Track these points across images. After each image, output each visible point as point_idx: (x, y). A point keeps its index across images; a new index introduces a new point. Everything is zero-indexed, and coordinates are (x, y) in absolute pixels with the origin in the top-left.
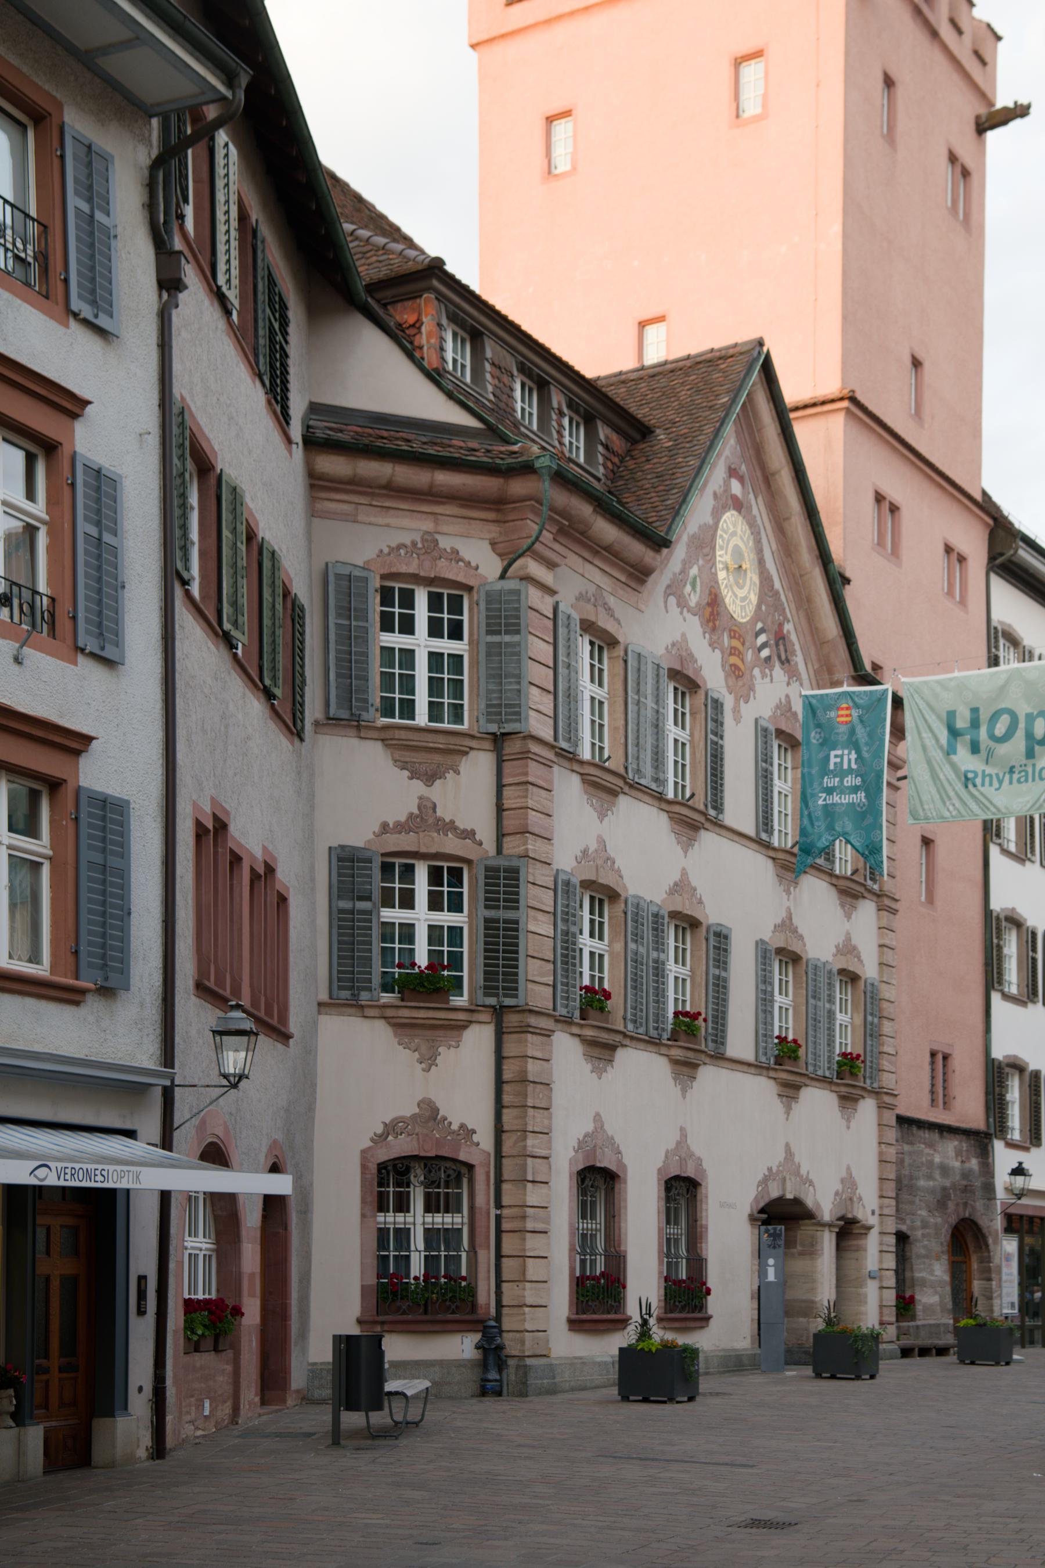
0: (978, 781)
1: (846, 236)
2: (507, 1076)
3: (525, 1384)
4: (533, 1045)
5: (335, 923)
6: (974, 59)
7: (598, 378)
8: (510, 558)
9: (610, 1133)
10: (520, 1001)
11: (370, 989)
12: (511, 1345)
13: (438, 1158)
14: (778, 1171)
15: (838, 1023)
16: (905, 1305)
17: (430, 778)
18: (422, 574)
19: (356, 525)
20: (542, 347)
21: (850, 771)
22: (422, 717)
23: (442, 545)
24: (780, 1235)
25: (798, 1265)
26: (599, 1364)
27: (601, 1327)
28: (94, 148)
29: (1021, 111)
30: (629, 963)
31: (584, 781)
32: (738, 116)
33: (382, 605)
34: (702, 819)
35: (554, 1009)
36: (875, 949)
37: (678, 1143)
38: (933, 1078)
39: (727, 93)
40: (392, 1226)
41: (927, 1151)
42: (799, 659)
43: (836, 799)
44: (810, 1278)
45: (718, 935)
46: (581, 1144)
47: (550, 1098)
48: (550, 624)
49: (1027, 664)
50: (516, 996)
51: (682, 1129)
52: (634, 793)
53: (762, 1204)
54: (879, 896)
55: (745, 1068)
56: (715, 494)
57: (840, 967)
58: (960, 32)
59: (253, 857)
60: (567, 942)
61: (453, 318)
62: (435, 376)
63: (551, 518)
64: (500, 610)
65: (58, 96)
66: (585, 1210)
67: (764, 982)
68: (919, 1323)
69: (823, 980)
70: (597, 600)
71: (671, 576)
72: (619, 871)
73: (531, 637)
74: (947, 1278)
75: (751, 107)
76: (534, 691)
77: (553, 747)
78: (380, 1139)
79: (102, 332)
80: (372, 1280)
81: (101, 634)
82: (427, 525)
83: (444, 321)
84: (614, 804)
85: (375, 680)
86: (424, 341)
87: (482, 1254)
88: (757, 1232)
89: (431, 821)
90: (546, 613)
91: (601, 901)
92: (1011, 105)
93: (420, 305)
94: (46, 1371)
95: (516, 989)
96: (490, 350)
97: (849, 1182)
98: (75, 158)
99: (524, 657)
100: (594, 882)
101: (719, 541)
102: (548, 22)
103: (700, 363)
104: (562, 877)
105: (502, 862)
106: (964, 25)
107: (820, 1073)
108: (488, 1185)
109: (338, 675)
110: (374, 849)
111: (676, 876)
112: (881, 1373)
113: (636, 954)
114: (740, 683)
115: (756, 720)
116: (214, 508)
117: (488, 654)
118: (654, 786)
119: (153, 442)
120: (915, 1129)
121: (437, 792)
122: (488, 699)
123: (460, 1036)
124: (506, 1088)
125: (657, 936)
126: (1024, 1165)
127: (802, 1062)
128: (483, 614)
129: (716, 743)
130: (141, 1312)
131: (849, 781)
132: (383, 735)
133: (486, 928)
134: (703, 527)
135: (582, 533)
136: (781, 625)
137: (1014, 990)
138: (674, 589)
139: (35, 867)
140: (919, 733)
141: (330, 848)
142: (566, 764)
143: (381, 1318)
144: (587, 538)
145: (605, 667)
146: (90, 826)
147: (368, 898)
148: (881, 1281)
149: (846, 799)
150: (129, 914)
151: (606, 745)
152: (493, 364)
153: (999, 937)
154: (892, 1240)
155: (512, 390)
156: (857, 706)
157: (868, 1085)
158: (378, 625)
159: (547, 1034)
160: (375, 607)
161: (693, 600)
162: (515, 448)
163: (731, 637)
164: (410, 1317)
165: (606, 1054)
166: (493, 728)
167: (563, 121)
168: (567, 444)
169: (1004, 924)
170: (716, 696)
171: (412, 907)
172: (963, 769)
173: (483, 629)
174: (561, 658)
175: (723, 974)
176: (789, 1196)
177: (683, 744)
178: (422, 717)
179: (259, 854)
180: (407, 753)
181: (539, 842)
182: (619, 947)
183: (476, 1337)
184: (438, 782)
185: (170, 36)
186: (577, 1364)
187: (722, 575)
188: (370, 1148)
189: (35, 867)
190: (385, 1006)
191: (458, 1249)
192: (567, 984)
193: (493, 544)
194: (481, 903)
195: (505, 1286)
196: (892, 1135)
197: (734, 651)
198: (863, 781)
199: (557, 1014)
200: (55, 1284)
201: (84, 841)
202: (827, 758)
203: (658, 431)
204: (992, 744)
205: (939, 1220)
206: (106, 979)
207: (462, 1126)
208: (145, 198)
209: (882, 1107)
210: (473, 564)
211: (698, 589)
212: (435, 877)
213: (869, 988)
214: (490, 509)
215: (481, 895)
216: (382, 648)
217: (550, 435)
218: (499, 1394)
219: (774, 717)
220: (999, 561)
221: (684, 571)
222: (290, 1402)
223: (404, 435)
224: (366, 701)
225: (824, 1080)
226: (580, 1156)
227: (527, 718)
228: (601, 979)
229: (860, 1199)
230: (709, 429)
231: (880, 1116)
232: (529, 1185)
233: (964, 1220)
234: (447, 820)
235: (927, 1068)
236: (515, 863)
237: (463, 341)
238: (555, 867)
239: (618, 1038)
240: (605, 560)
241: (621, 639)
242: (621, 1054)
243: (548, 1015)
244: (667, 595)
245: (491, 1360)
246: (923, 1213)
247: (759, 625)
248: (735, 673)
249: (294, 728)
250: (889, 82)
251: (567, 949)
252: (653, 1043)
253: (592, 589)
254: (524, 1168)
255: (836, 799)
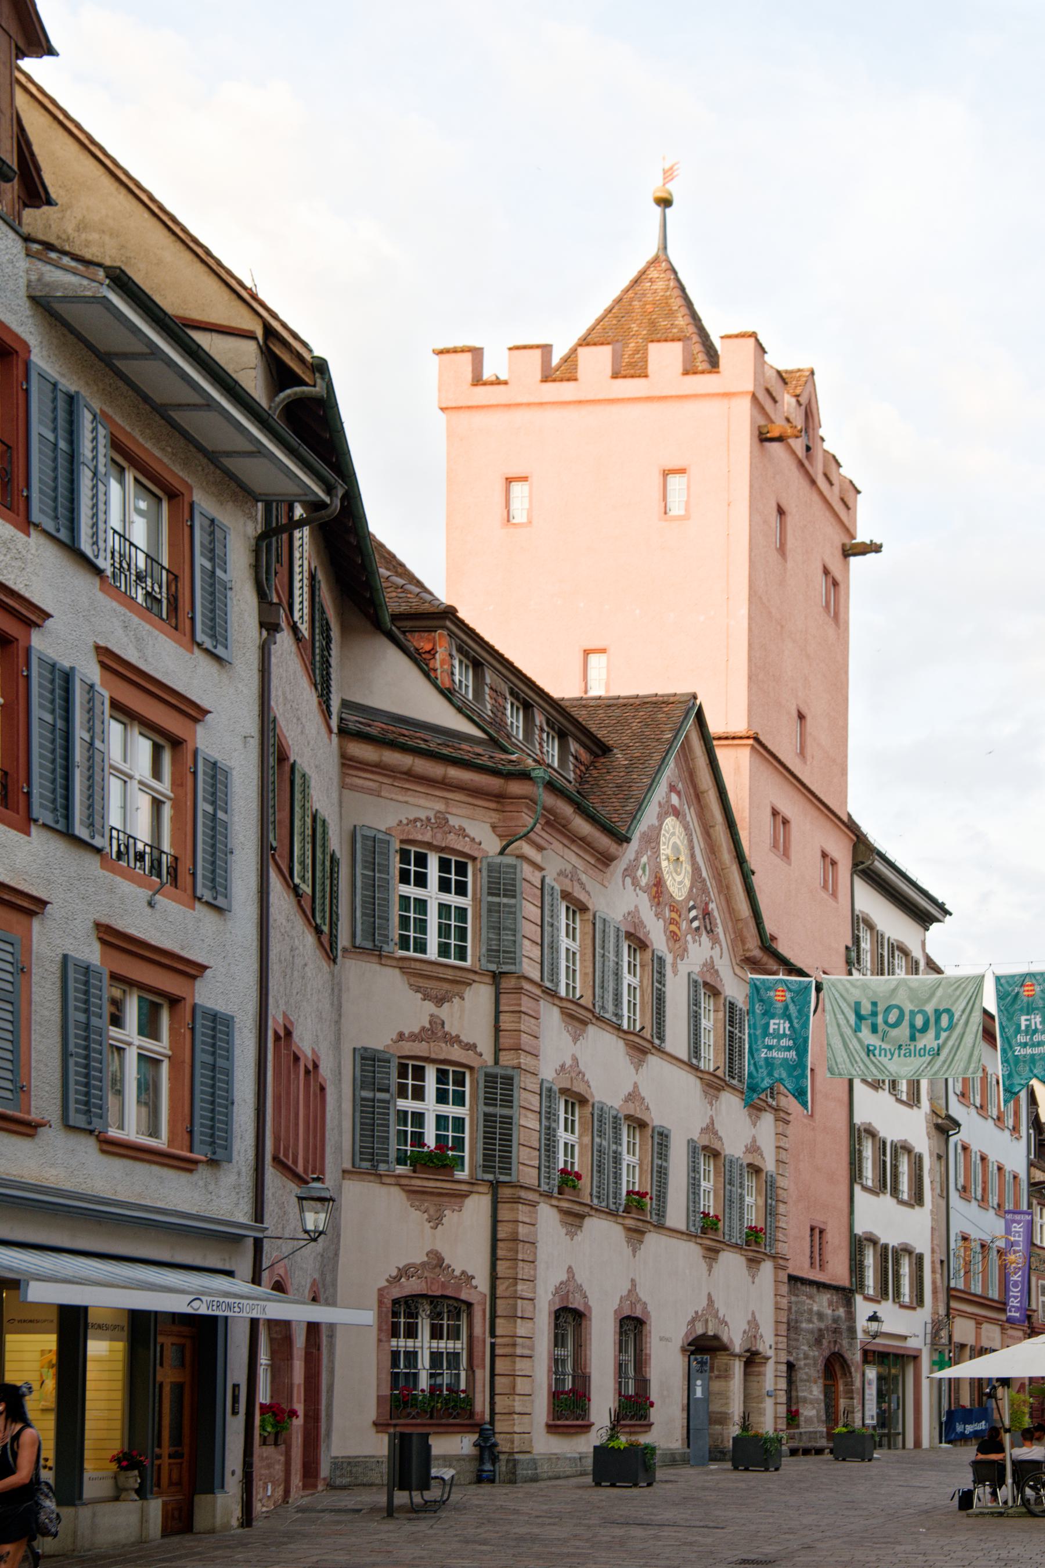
0: (877, 1052)
1: (750, 618)
2: (501, 1235)
3: (514, 1473)
4: (522, 1213)
5: (358, 1108)
6: (841, 503)
7: (563, 699)
8: (509, 840)
9: (579, 1282)
10: (514, 1179)
11: (387, 1162)
12: (503, 1444)
13: (443, 1297)
14: (703, 1315)
15: (702, 1189)
16: (792, 1417)
17: (440, 1001)
18: (435, 843)
19: (380, 799)
20: (472, 631)
21: (784, 1035)
22: (432, 952)
23: (451, 823)
24: (706, 1363)
25: (716, 1386)
26: (570, 1459)
27: (572, 1430)
28: (216, 522)
29: (876, 548)
30: (595, 1153)
31: (562, 1013)
32: (666, 513)
33: (401, 862)
34: (649, 1046)
35: (539, 1186)
36: (773, 1149)
37: (630, 1291)
38: (812, 1247)
39: (657, 494)
40: (402, 1350)
41: (808, 1301)
42: (720, 930)
43: (774, 1054)
44: (724, 1396)
45: (661, 1134)
46: (557, 1290)
47: (535, 1254)
48: (539, 892)
49: (914, 977)
50: (510, 1175)
51: (633, 1280)
52: (599, 1023)
53: (690, 1339)
54: (776, 1110)
55: (679, 1236)
56: (660, 803)
57: (749, 1161)
58: (831, 484)
59: (306, 1056)
60: (549, 1134)
61: (460, 650)
62: (448, 694)
63: (543, 815)
64: (499, 878)
65: (189, 481)
66: (559, 1340)
67: (694, 1171)
68: (802, 1430)
69: (736, 1171)
70: (573, 876)
71: (627, 861)
72: (587, 1082)
73: (524, 902)
74: (822, 1397)
75: (676, 508)
76: (526, 942)
77: (540, 986)
78: (395, 1280)
79: (218, 659)
80: (386, 1391)
81: (214, 887)
82: (440, 806)
83: (454, 653)
84: (584, 1031)
85: (395, 921)
86: (438, 665)
87: (479, 1373)
88: (686, 1360)
89: (440, 1034)
90: (535, 884)
91: (573, 1104)
92: (868, 542)
93: (434, 638)
94: (159, 1457)
95: (510, 1169)
96: (489, 677)
97: (753, 1323)
98: (202, 528)
99: (519, 916)
100: (569, 1090)
101: (662, 839)
102: (508, 406)
103: (647, 703)
104: (546, 1085)
105: (499, 1071)
106: (834, 479)
107: (733, 1241)
108: (484, 1319)
109: (364, 914)
110: (391, 1052)
111: (630, 1088)
112: (782, 1467)
113: (600, 1146)
114: (677, 946)
115: (689, 974)
116: (288, 789)
117: (489, 911)
118: (614, 1019)
119: (254, 743)
120: (799, 1284)
121: (444, 1012)
122: (489, 945)
123: (463, 1202)
124: (500, 1244)
125: (616, 1133)
126: (878, 1314)
127: (720, 1232)
128: (485, 880)
129: (660, 990)
130: (235, 1413)
131: (784, 1042)
132: (401, 964)
133: (485, 1121)
134: (651, 827)
135: (563, 826)
136: (707, 904)
137: (870, 1183)
138: (630, 872)
139: (157, 1062)
140: (835, 1015)
141: (354, 1049)
142: (549, 999)
143: (394, 1422)
144: (567, 830)
145: (578, 926)
146: (204, 1034)
147: (387, 1091)
148: (776, 1398)
149: (781, 1055)
150: (233, 1103)
151: (578, 985)
152: (491, 688)
153: (860, 1144)
154: (784, 1368)
155: (505, 709)
156: (790, 990)
157: (767, 1251)
158: (398, 878)
159: (534, 1205)
160: (396, 865)
161: (644, 881)
162: (513, 757)
163: (671, 911)
164: (419, 1421)
165: (577, 1221)
166: (493, 967)
167: (520, 483)
168: (457, 682)
169: (863, 1134)
170: (660, 954)
171: (423, 1100)
172: (866, 1043)
173: (485, 891)
174: (547, 919)
175: (664, 1164)
176: (711, 1333)
177: (635, 988)
178: (432, 952)
179: (309, 1054)
180: (421, 980)
181: (529, 1058)
182: (587, 1140)
183: (475, 1437)
184: (446, 1005)
185: (286, 455)
186: (554, 1459)
187: (664, 864)
188: (386, 1287)
189: (157, 1062)
190: (399, 1176)
191: (458, 1368)
192: (549, 1167)
193: (494, 827)
194: (481, 1101)
195: (497, 1398)
196: (784, 1289)
197: (672, 921)
198: (795, 1043)
199: (541, 1189)
200: (167, 1389)
201: (199, 1046)
202: (767, 1025)
203: (615, 750)
204: (887, 1029)
205: (816, 1353)
206: (214, 1153)
207: (463, 1273)
208: (253, 561)
209: (778, 1267)
210: (477, 840)
211: (647, 873)
212: (442, 1077)
213: (769, 1179)
214: (491, 800)
215: (481, 1095)
216: (401, 896)
217: (533, 745)
218: (493, 1481)
219: (701, 972)
220: (861, 867)
221: (636, 859)
222: (320, 1488)
223: (422, 736)
224: (387, 936)
225: (736, 1246)
226: (557, 1299)
227: (521, 963)
228: (573, 1164)
229: (761, 1336)
230: (657, 757)
231: (776, 1275)
232: (519, 1320)
233: (834, 1354)
234: (454, 1034)
235: (808, 1239)
236: (510, 1072)
237: (467, 667)
238: (541, 1077)
239: (587, 1210)
240: (580, 847)
241: (590, 906)
242: (588, 1222)
243: (535, 1190)
244: (624, 876)
245: (486, 1456)
246: (805, 1348)
247: (691, 903)
248: (674, 937)
249: (330, 951)
250: (781, 512)
251: (549, 1140)
252: (612, 1214)
253: (569, 868)
254: (515, 1307)
255: (774, 1054)
